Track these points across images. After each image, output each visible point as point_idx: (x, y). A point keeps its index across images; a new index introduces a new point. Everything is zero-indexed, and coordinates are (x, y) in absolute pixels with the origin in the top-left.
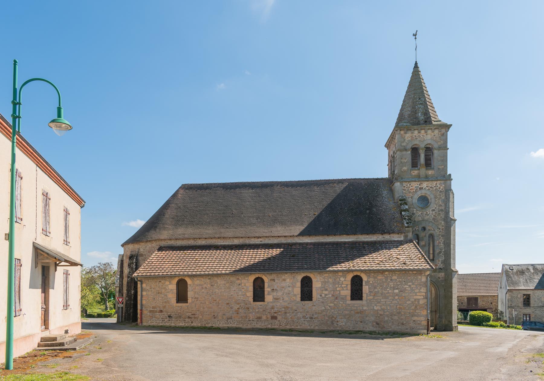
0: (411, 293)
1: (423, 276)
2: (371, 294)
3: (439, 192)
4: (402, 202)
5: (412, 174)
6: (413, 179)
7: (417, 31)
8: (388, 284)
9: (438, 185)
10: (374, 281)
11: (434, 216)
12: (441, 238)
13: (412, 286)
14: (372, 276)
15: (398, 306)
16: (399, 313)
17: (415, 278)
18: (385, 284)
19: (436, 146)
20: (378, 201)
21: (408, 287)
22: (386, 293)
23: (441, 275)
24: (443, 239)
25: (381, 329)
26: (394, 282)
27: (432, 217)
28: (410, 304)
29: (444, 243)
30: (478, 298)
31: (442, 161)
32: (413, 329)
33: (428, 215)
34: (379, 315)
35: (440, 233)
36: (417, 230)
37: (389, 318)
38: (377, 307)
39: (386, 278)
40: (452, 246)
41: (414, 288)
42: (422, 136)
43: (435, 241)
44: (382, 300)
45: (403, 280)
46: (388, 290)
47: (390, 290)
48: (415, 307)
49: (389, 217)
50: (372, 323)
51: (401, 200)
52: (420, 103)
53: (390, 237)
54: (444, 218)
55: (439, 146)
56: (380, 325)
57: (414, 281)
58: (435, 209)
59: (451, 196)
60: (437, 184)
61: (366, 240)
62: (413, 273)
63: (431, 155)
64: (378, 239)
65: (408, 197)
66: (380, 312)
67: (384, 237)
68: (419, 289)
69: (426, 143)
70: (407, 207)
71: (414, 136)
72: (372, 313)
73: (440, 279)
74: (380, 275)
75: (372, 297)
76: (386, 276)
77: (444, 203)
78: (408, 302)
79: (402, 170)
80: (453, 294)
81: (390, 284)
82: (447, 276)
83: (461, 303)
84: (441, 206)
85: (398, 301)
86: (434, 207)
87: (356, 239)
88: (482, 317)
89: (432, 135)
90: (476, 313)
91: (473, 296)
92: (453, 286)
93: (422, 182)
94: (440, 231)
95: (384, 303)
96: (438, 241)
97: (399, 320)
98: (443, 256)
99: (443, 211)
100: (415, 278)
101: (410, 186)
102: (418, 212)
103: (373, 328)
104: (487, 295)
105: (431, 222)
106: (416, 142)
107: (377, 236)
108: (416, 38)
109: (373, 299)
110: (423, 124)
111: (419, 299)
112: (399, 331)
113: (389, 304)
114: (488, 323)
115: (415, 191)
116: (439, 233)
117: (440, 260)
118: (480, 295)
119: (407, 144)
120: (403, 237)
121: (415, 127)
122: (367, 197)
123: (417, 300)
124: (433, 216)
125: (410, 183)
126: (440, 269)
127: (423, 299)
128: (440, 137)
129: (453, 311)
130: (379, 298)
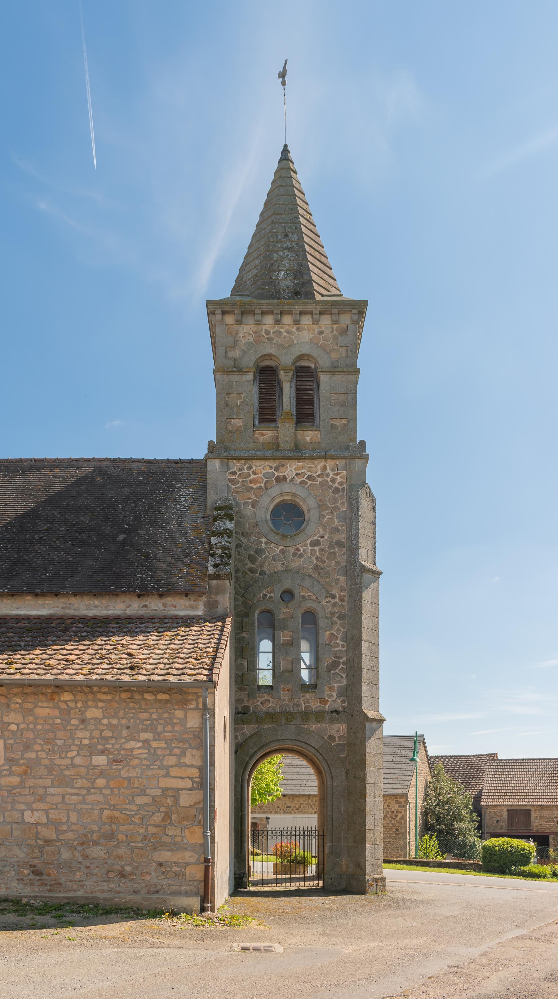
0: (148, 767)
1: (193, 709)
2: (13, 769)
3: (333, 492)
4: (219, 512)
5: (257, 438)
6: (258, 453)
7: (286, 61)
8: (72, 736)
9: (328, 470)
10: (22, 723)
11: (317, 559)
12: (336, 623)
13: (155, 744)
14: (18, 706)
15: (106, 813)
16: (111, 836)
17: (166, 715)
18: (60, 734)
19: (324, 361)
20: (160, 512)
21: (139, 748)
22: (67, 766)
23: (336, 729)
24: (344, 628)
25: (49, 891)
26: (93, 727)
27: (311, 562)
28: (147, 805)
29: (345, 639)
30: (530, 810)
31: (343, 404)
32: (157, 892)
33: (301, 556)
34: (40, 843)
35: (336, 610)
36: (271, 597)
37: (77, 854)
38: (35, 813)
39: (66, 713)
40: (365, 646)
41: (159, 752)
42: (285, 334)
43: (321, 632)
44: (51, 790)
45: (124, 722)
46: (70, 754)
47: (78, 754)
48: (164, 817)
49: (174, 553)
50: (16, 867)
51: (222, 507)
52: (285, 246)
53: (165, 605)
54: (346, 566)
55: (332, 363)
56: (45, 877)
57: (160, 728)
58: (321, 540)
59: (364, 503)
60: (325, 468)
61: (92, 613)
62: (159, 701)
63: (312, 390)
64: (129, 612)
65: (245, 503)
66: (49, 834)
67: (146, 606)
68: (179, 756)
69: (296, 352)
70: (230, 525)
71: (263, 333)
72: (15, 834)
73: (335, 741)
74: (45, 704)
75: (15, 780)
76: (64, 706)
77: (346, 522)
78: (139, 800)
79: (230, 427)
80: (368, 786)
81: (80, 734)
82: (354, 733)
83: (495, 822)
84: (338, 530)
85: (105, 796)
86: (319, 535)
87: (63, 608)
88: (508, 852)
89: (314, 330)
90: (497, 844)
91: (519, 805)
92: (367, 762)
93: (284, 462)
94: (335, 604)
95: (59, 799)
96: (328, 633)
97: (110, 861)
98: (342, 677)
99: (344, 547)
100: (166, 715)
101: (251, 471)
102: (272, 546)
103: (21, 886)
104: (550, 805)
105: (310, 576)
106: (271, 350)
107: (124, 602)
108: (284, 84)
109: (22, 784)
110: (289, 298)
111: (177, 790)
112: (105, 899)
113: (75, 805)
114: (522, 868)
115: (263, 485)
116: (333, 608)
117: (334, 687)
118: (534, 803)
119: (244, 352)
120: (204, 605)
121: (265, 304)
122: (135, 502)
123: (170, 793)
124: (314, 559)
125: (249, 462)
126: (334, 714)
127: (190, 789)
128: (335, 338)
129: (367, 834)
130: (40, 782)
